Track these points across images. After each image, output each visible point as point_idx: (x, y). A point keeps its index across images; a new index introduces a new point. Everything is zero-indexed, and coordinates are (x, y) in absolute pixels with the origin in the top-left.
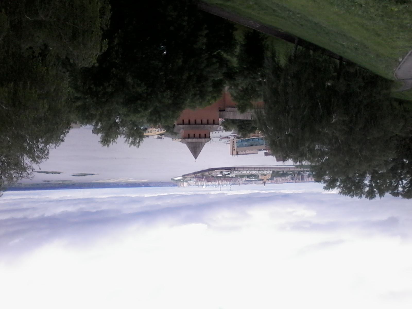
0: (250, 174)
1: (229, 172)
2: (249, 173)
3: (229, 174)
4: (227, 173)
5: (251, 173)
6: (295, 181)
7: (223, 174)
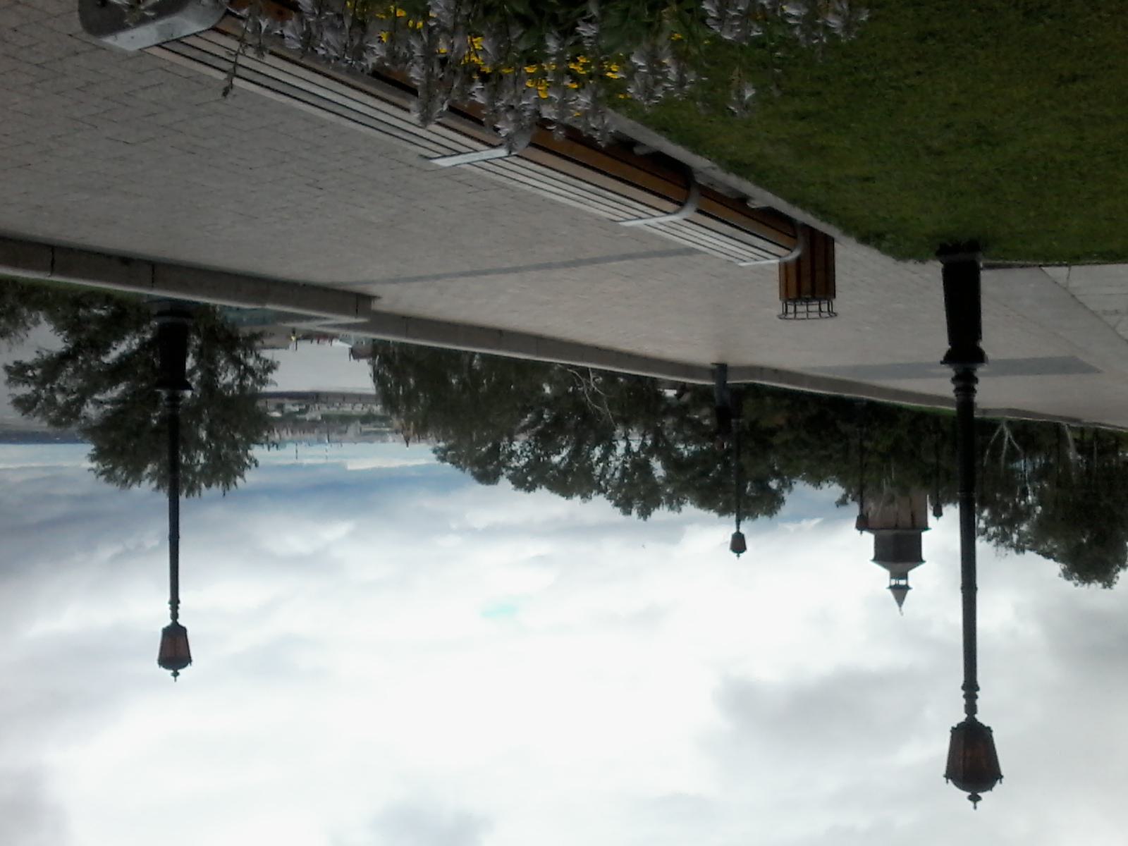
0: (364, 414)
1: (304, 407)
2: (359, 410)
3: (301, 412)
4: (297, 409)
5: (366, 410)
6: (308, 40)
7: (286, 412)
